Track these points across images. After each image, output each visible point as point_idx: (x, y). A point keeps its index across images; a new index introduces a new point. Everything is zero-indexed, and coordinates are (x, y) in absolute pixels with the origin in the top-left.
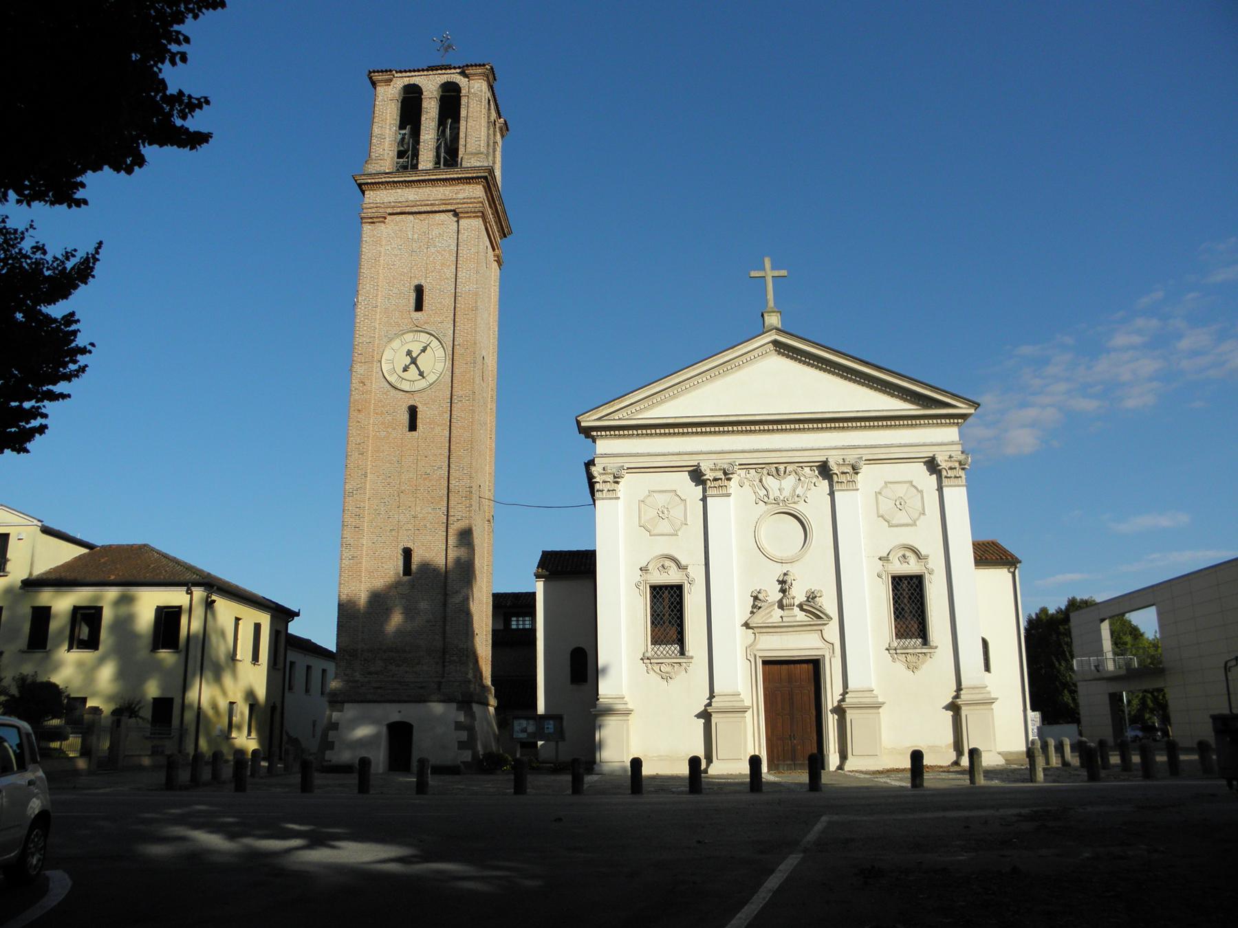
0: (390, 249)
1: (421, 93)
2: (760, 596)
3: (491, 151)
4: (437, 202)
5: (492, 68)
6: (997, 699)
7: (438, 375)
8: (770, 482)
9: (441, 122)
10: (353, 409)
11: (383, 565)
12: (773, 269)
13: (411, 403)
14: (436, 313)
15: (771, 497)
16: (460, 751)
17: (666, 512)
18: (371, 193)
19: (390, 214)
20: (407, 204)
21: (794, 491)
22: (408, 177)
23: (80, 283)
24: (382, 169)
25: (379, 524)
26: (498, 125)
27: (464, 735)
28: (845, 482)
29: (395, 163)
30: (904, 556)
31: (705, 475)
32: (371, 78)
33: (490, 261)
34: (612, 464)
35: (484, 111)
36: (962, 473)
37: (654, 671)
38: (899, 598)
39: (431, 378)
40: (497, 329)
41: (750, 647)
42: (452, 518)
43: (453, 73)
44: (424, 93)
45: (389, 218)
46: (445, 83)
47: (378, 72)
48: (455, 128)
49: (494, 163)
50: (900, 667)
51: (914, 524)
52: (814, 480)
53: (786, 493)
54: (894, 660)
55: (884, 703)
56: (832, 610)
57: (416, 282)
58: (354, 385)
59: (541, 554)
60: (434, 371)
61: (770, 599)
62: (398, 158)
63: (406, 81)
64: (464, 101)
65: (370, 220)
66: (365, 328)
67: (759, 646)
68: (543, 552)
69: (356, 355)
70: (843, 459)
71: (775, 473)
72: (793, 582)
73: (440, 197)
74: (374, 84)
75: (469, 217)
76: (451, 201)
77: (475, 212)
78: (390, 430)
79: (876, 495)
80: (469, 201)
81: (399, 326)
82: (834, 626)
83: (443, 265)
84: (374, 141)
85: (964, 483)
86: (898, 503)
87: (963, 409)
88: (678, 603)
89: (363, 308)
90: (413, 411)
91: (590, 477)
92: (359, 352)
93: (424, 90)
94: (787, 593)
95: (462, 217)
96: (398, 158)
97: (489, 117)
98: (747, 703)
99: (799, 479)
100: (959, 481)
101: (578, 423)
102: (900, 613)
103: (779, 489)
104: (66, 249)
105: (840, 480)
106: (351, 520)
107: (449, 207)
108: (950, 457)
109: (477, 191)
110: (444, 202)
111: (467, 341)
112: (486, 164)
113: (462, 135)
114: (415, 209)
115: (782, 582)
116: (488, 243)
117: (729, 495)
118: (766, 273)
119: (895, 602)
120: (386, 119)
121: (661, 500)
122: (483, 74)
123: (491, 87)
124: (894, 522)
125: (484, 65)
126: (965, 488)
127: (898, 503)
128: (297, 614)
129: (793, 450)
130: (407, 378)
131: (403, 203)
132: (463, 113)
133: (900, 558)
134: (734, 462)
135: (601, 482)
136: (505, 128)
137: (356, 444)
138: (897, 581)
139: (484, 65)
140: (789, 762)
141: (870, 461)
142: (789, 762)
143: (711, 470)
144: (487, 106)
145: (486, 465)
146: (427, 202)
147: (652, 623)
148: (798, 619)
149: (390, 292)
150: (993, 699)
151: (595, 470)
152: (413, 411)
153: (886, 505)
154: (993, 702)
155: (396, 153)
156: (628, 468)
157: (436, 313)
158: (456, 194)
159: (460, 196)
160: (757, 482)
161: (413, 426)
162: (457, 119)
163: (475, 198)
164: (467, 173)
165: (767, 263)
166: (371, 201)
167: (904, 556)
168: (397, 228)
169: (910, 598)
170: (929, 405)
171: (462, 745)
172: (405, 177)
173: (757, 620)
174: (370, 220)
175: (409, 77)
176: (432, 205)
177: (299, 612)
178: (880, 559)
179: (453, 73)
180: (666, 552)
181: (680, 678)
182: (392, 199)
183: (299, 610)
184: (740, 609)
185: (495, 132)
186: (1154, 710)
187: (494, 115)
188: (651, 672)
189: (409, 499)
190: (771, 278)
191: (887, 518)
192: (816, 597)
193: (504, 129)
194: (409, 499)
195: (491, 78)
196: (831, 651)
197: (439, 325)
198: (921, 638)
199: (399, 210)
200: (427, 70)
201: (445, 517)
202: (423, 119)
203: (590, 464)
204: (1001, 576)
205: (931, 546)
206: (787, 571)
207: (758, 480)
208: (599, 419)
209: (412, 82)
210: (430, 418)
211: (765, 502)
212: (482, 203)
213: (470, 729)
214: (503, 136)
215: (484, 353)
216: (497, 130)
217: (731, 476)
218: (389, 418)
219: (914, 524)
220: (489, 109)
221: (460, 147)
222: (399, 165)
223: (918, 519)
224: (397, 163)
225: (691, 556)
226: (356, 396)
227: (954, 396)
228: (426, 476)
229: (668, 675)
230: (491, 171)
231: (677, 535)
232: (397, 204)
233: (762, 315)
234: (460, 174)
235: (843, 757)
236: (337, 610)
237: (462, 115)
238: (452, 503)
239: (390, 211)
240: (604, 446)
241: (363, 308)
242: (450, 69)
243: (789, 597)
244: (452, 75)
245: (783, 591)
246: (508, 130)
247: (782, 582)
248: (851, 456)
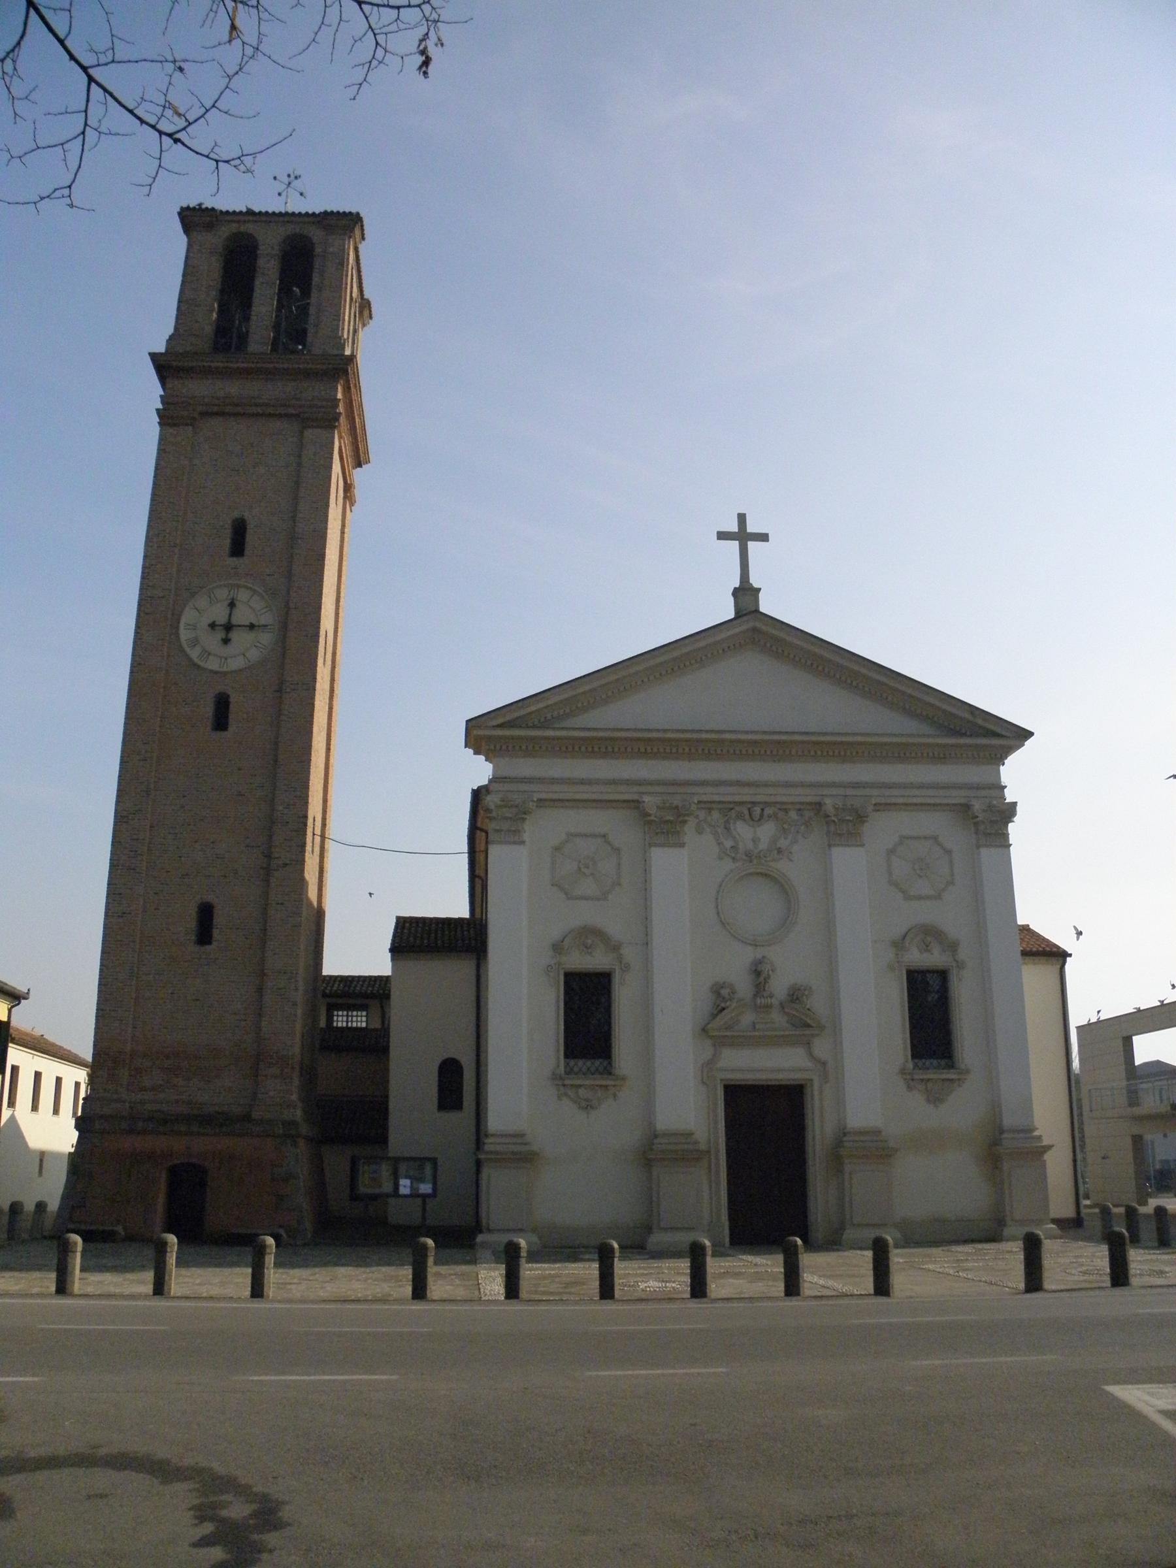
8: (743, 830)
9: (284, 291)
44: (261, 248)
51: (938, 897)
53: (763, 845)
54: (910, 1088)
59: (395, 920)
64: (317, 263)
68: (398, 918)
71: (747, 817)
104: (1099, 1012)
127: (916, 867)
132: (316, 279)
177: (28, 993)
206: (764, 957)
208: (501, 726)
217: (686, 818)
219: (938, 897)
231: (605, 899)
236: (393, 927)
243: (765, 994)
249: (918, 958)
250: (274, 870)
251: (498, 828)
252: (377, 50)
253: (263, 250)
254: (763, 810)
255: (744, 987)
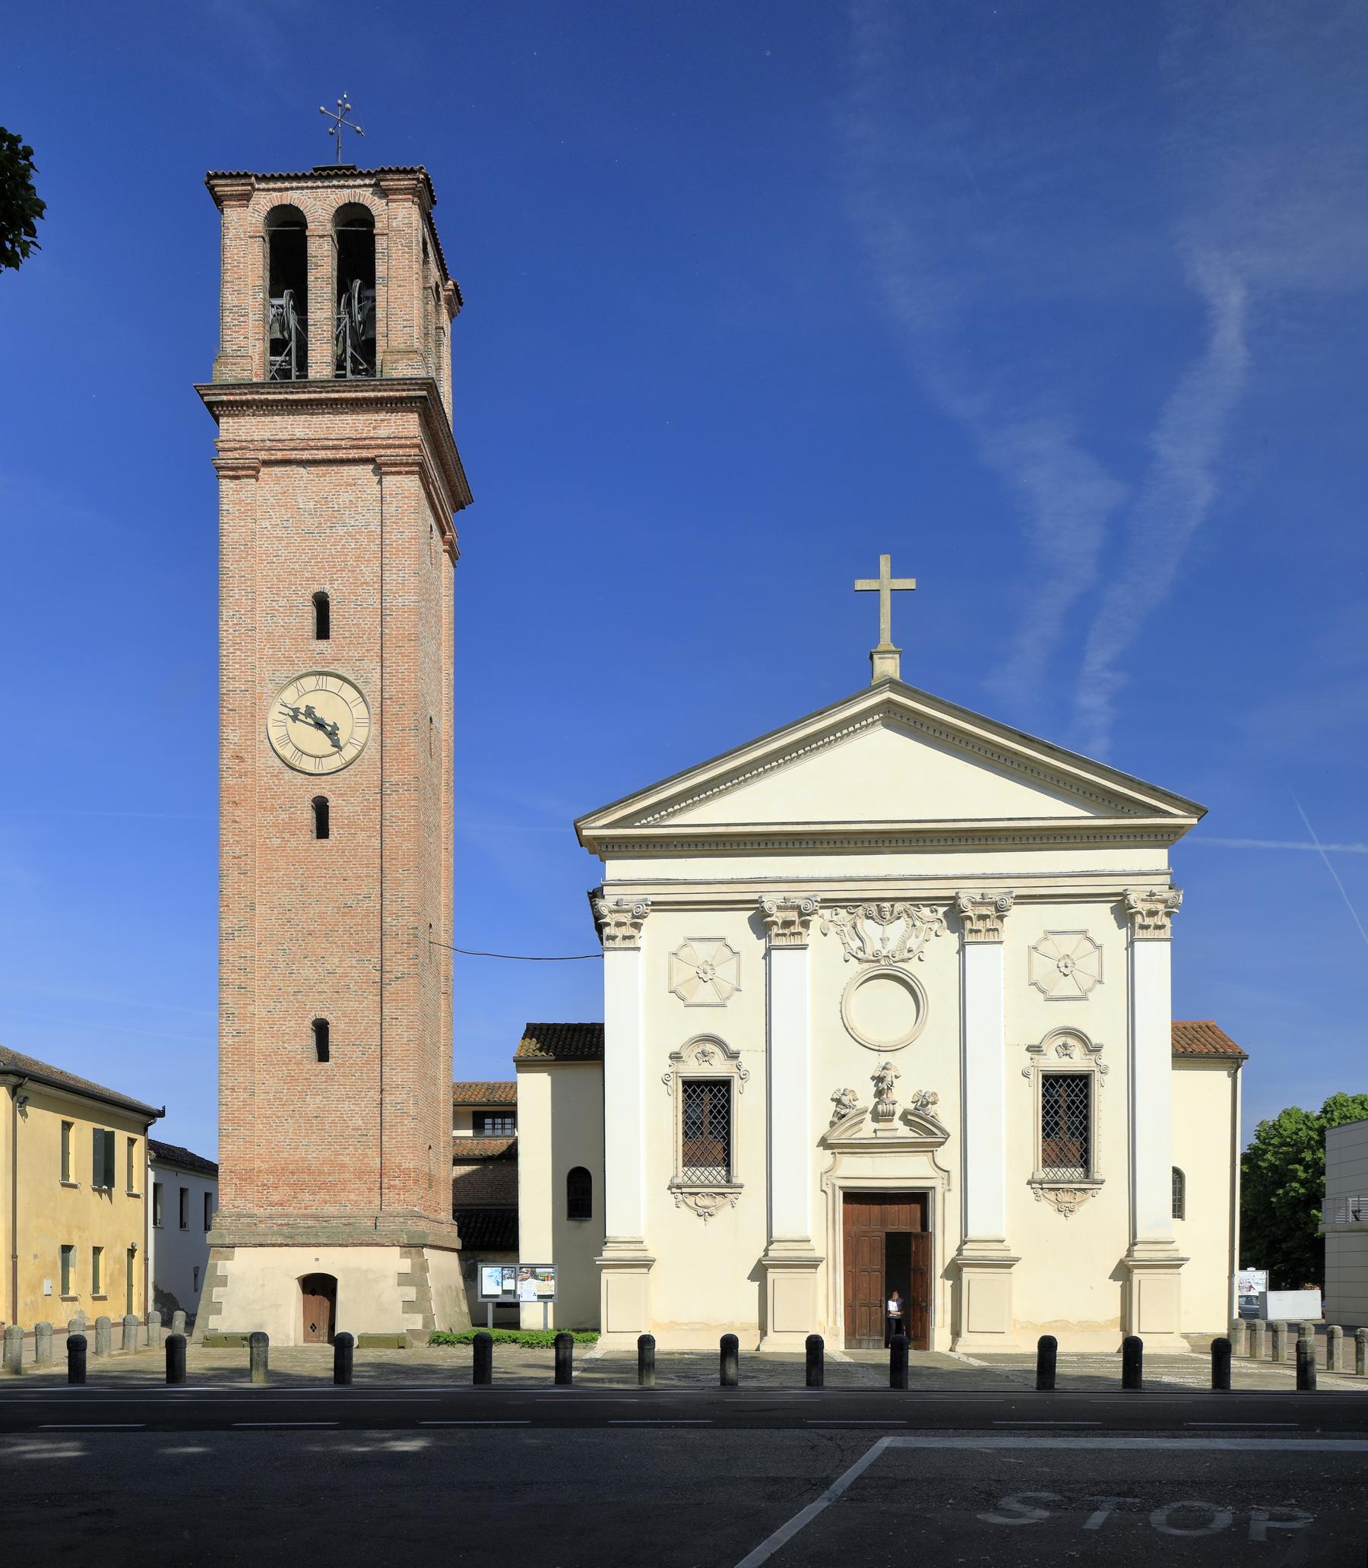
0: (269, 527)
1: (304, 225)
2: (845, 1100)
3: (432, 345)
4: (343, 443)
5: (427, 179)
6: (1187, 1260)
7: (360, 748)
8: (868, 927)
10: (225, 800)
11: (286, 1045)
12: (895, 575)
13: (317, 792)
14: (351, 643)
15: (869, 951)
16: (406, 1315)
17: (710, 972)
18: (230, 420)
19: (267, 463)
20: (292, 444)
21: (904, 942)
22: (292, 393)
23: (1316, 839)
24: (244, 376)
25: (277, 983)
26: (443, 294)
27: (411, 1293)
28: (983, 930)
29: (267, 364)
30: (1065, 1046)
31: (770, 916)
32: (211, 189)
33: (436, 552)
34: (632, 896)
35: (417, 267)
36: (1167, 921)
37: (686, 1203)
38: (1052, 1107)
39: (349, 752)
40: (452, 671)
41: (826, 1172)
42: (388, 975)
43: (360, 186)
44: (311, 226)
45: (264, 470)
46: (346, 205)
47: (223, 176)
48: (368, 298)
49: (439, 368)
50: (1046, 1208)
52: (936, 926)
55: (1017, 1260)
56: (954, 1130)
57: (317, 588)
58: (225, 761)
60: (352, 741)
61: (859, 1105)
62: (272, 354)
63: (276, 199)
64: (380, 244)
65: (231, 473)
66: (237, 666)
67: (841, 1172)
69: (225, 710)
70: (982, 895)
71: (875, 914)
72: (894, 1079)
73: (348, 433)
74: (219, 201)
75: (399, 473)
76: (367, 442)
77: (407, 464)
78: (287, 836)
79: (1030, 954)
80: (397, 443)
81: (292, 663)
82: (953, 1146)
83: (358, 558)
84: (228, 318)
85: (1168, 936)
86: (1062, 964)
87: (1182, 818)
88: (723, 1107)
89: (231, 631)
90: (321, 807)
91: (597, 916)
92: (230, 707)
93: (309, 219)
94: (885, 1096)
95: (387, 474)
96: (272, 354)
97: (426, 278)
98: (819, 1253)
99: (914, 925)
100: (1161, 934)
101: (578, 831)
102: (1052, 1129)
103: (881, 939)
105: (974, 928)
106: (233, 976)
107: (365, 454)
108: (1152, 894)
109: (408, 425)
110: (355, 442)
111: (403, 692)
112: (422, 374)
113: (380, 313)
114: (306, 455)
115: (879, 1079)
116: (432, 521)
117: (804, 947)
118: (881, 583)
119: (1046, 1113)
120: (246, 276)
121: (703, 952)
122: (412, 191)
123: (427, 218)
124: (1055, 993)
125: (412, 171)
126: (1169, 944)
127: (1062, 964)
128: (161, 1114)
129: (905, 879)
130: (310, 752)
131: (287, 443)
132: (380, 269)
133: (1059, 1049)
134: (815, 896)
135: (613, 923)
136: (456, 300)
137: (235, 857)
138: (1052, 1082)
139: (412, 171)
140: (877, 1338)
141: (1024, 899)
142: (877, 1338)
143: (779, 908)
144: (422, 255)
145: (440, 893)
146: (326, 443)
147: (685, 1134)
148: (899, 1134)
149: (274, 604)
150: (1182, 1259)
151: (605, 905)
152: (321, 807)
153: (1044, 969)
154: (1181, 1265)
155: (268, 345)
156: (653, 903)
157: (351, 643)
158: (374, 428)
159: (383, 432)
160: (848, 929)
161: (322, 830)
162: (370, 282)
163: (406, 438)
164: (391, 390)
165: (885, 563)
166: (231, 436)
167: (1065, 1046)
168: (278, 488)
169: (1069, 1108)
170: (1126, 810)
171: (409, 1306)
172: (286, 393)
173: (837, 1136)
174: (231, 473)
175: (280, 190)
176: (334, 448)
177: (164, 1111)
178: (1028, 1049)
179: (360, 186)
180: (707, 1031)
181: (725, 1214)
182: (267, 435)
183: (164, 1108)
184: (817, 1119)
185: (437, 305)
186: (245, 404)
187: (435, 274)
188: (683, 1206)
189: (322, 946)
190: (889, 592)
191: (1044, 986)
192: (928, 1103)
193: (455, 300)
194: (322, 946)
195: (427, 198)
196: (945, 1182)
197: (358, 663)
198: (1082, 1167)
199: (279, 455)
200: (311, 177)
201: (378, 974)
202: (311, 278)
203: (595, 894)
204: (1215, 1083)
205: (1106, 1030)
206: (887, 1064)
207: (849, 925)
209: (286, 202)
210: (348, 818)
211: (859, 959)
212: (418, 446)
213: (422, 1287)
214: (452, 315)
215: (432, 712)
216: (442, 302)
218: (284, 816)
220: (426, 262)
221: (378, 337)
222: (275, 368)
223: (1090, 990)
224: (272, 364)
225: (741, 1035)
226: (229, 780)
227: (1152, 791)
228: (347, 910)
229: (705, 1210)
230: (431, 386)
231: (723, 1006)
232: (274, 443)
233: (871, 657)
234: (380, 391)
235: (956, 1333)
237: (378, 274)
238: (388, 953)
239: (263, 455)
240: (616, 869)
241: (231, 631)
242: (353, 176)
243: (887, 1102)
244: (358, 191)
245: (879, 1093)
246: (461, 304)
247: (879, 1079)
248: (995, 891)
249: (1057, 1063)
250: (387, 984)
251: (1160, 923)
252: (825, 1252)
253: (312, 227)
254: (892, 906)
255: (866, 1098)
